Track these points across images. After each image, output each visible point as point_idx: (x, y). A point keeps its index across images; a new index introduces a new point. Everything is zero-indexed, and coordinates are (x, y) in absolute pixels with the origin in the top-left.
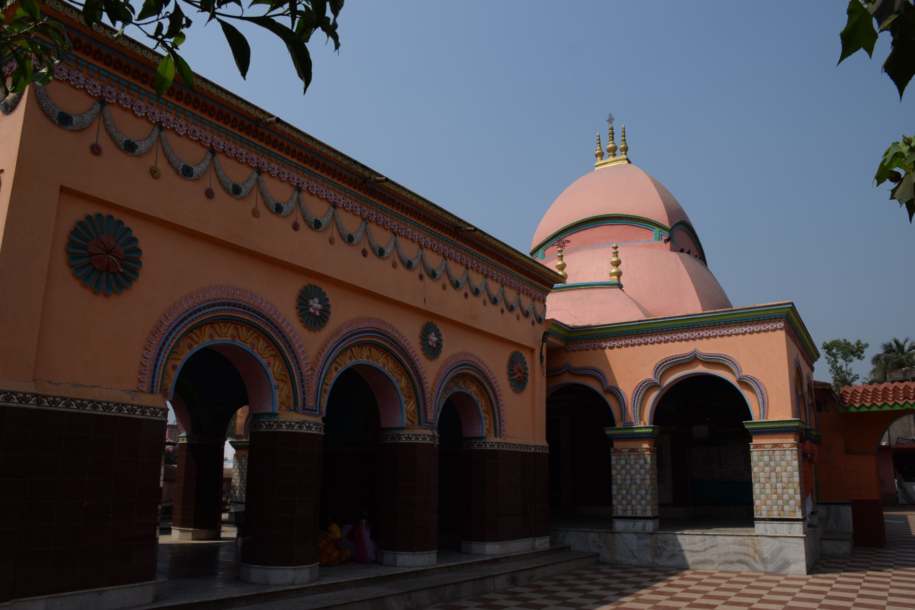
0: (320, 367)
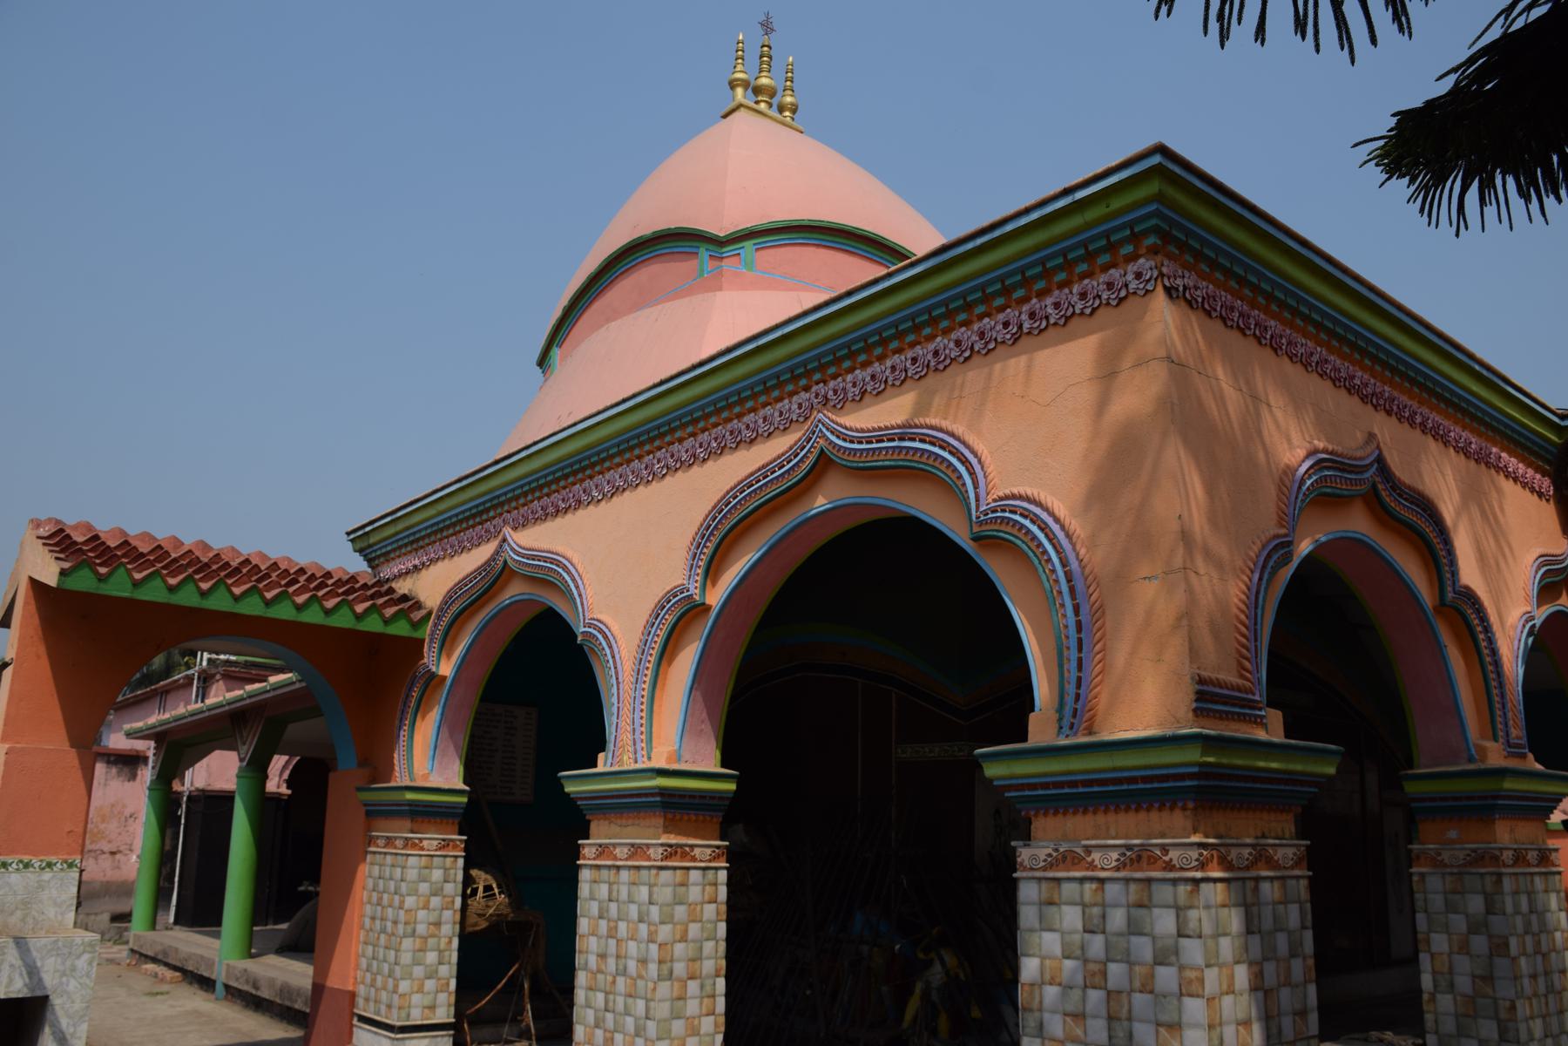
0: (1264, 547)
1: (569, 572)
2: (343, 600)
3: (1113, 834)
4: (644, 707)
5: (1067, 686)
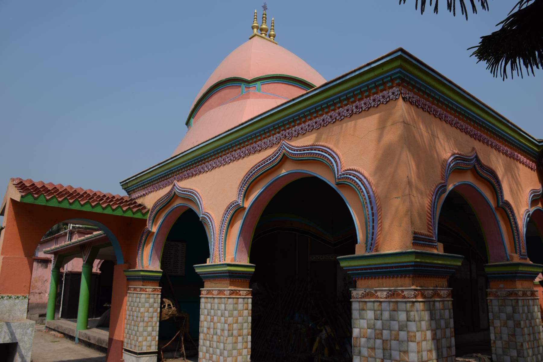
1: (197, 196)
2: (119, 206)
3: (385, 286)
4: (223, 242)
5: (369, 235)
